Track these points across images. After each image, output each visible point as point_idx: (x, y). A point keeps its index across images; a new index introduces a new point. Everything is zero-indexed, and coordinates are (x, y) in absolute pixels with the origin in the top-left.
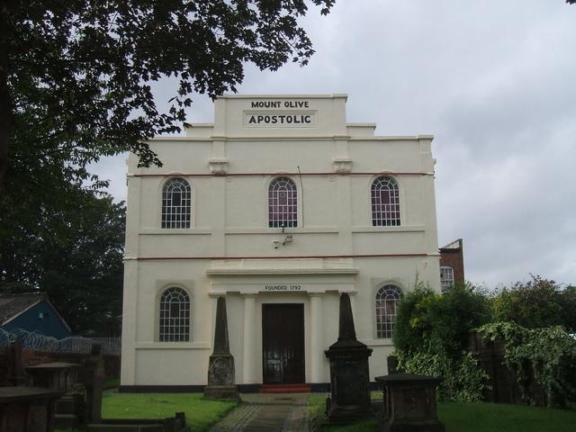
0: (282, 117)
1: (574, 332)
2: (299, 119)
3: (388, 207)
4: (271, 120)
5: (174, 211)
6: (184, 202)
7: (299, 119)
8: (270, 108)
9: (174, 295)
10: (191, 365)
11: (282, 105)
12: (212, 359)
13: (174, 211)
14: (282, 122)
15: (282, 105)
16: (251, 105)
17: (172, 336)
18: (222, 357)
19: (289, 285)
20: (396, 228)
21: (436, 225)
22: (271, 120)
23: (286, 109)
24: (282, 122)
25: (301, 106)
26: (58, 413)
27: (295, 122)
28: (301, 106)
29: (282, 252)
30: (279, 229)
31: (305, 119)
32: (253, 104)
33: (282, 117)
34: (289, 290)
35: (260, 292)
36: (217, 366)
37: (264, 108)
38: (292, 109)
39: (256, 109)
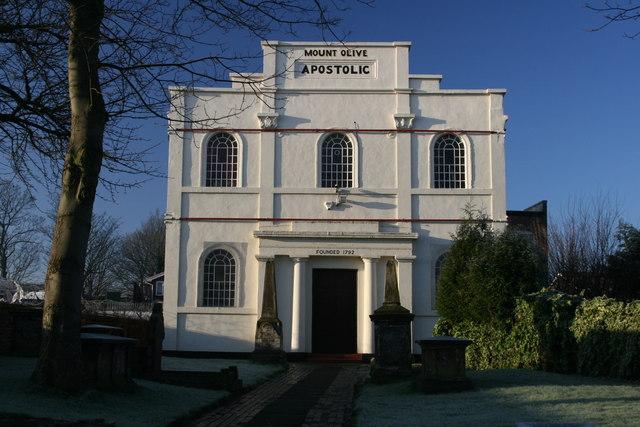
0: (338, 67)
1: (2, 303)
2: (356, 69)
3: (452, 167)
4: (326, 70)
5: (219, 168)
6: (228, 276)
7: (356, 69)
8: (325, 57)
9: (222, 140)
10: (242, 323)
11: (338, 53)
12: (259, 324)
13: (219, 168)
14: (338, 72)
15: (338, 53)
16: (304, 52)
17: (216, 301)
18: (272, 317)
19: (342, 249)
20: (459, 190)
21: (506, 176)
22: (326, 70)
23: (342, 58)
24: (338, 72)
25: (359, 54)
26: (393, 183)
27: (353, 72)
28: (359, 54)
29: (342, 215)
30: (334, 190)
31: (363, 70)
32: (306, 52)
33: (338, 67)
34: (341, 254)
35: (311, 256)
36: (264, 330)
37: (318, 57)
38: (349, 58)
39: (310, 57)
